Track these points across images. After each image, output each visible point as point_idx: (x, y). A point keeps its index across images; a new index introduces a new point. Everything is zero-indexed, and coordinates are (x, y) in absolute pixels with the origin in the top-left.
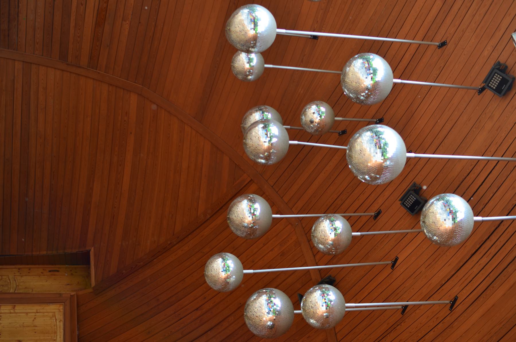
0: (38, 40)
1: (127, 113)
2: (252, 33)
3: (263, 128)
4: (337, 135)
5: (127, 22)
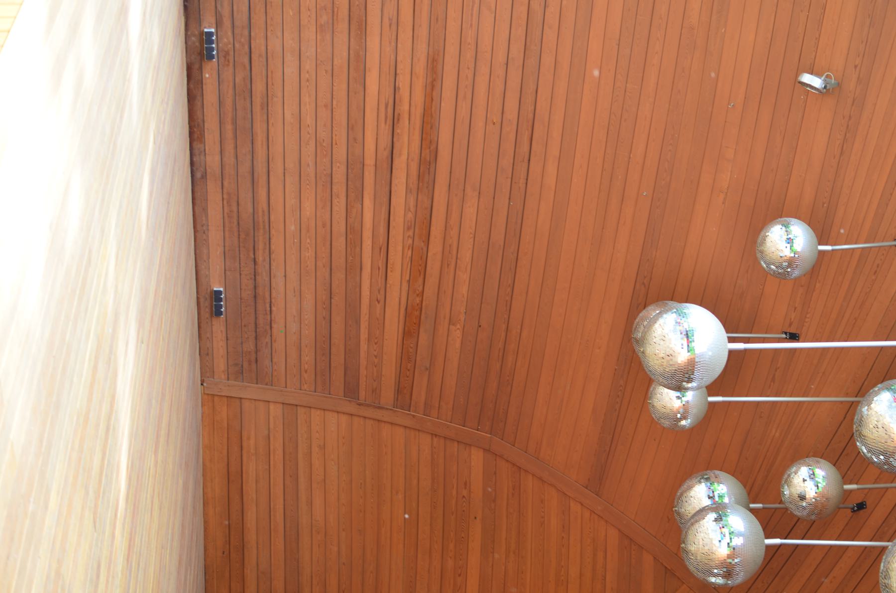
0: (306, 366)
1: (465, 484)
2: (682, 357)
3: (716, 520)
4: (850, 511)
5: (458, 326)
